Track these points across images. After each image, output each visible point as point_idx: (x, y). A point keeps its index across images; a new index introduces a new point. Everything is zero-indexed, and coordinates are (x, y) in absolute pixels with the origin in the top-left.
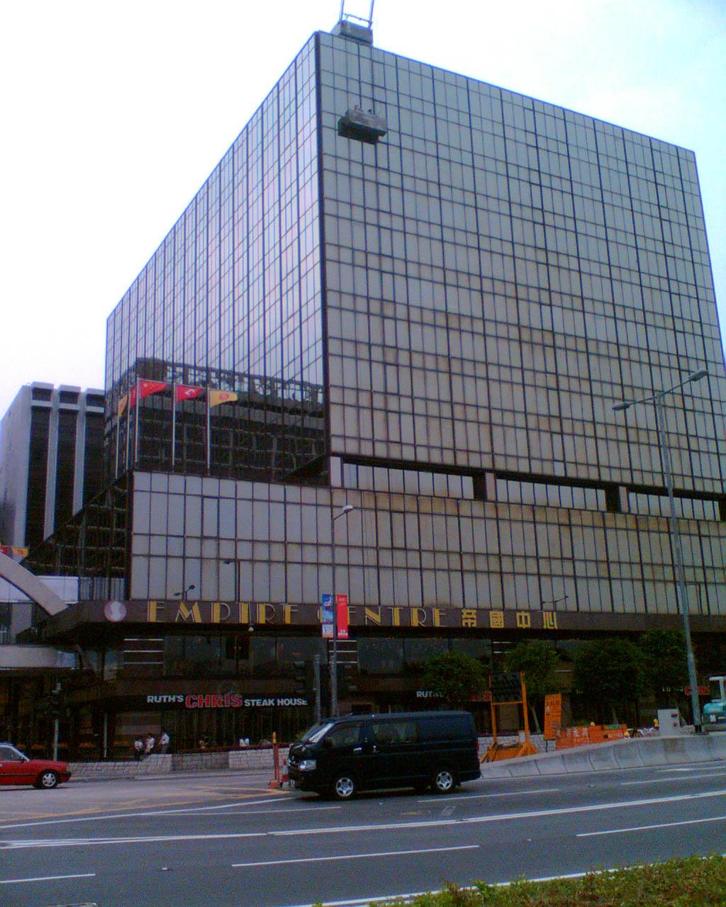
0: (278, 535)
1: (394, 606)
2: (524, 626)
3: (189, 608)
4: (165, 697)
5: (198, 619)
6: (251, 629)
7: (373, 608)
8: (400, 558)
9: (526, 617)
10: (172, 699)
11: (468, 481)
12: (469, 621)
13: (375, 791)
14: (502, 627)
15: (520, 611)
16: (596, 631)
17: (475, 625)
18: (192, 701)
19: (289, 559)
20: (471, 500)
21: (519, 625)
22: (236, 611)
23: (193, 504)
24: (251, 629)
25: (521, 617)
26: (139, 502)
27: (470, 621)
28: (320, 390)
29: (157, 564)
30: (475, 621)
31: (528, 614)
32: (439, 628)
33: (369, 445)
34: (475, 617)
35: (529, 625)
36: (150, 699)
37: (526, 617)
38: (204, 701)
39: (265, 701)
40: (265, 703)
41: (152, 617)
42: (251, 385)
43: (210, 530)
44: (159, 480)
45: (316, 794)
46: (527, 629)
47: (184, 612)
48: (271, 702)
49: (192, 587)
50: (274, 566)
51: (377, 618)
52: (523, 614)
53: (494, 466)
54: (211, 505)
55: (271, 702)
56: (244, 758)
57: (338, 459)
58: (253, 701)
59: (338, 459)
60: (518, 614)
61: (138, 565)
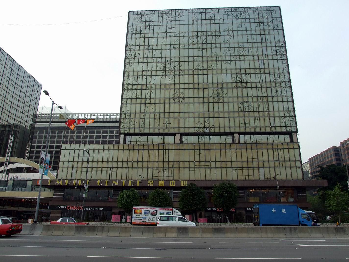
0: (100, 160)
1: (67, 179)
2: (172, 185)
3: (59, 181)
4: (61, 206)
5: (61, 184)
6: (278, 188)
7: (116, 180)
8: (140, 164)
9: (174, 182)
10: (213, 209)
11: (230, 137)
12: (150, 184)
13: (289, 240)
14: (163, 186)
15: (171, 180)
16: (257, 187)
17: (152, 185)
18: (69, 208)
19: (270, 166)
20: (179, 144)
21: (170, 185)
22: (72, 182)
23: (77, 152)
24: (76, 187)
25: (171, 182)
26: (62, 152)
27: (150, 184)
28: (119, 114)
29: (65, 169)
30: (153, 184)
31: (175, 182)
32: (50, 186)
33: (238, 128)
34: (153, 183)
35: (174, 185)
36: (57, 207)
37: (174, 182)
38: (72, 208)
39: (90, 208)
40: (90, 209)
41: (106, 185)
42: (97, 116)
43: (81, 159)
44: (68, 146)
45: (5, 236)
46: (173, 187)
47: (58, 182)
48: (92, 209)
49: (278, 175)
50: (144, 169)
51: (116, 184)
52: (172, 181)
53: (266, 131)
54: (81, 152)
55: (92, 209)
56: (214, 225)
57: (237, 134)
58: (86, 208)
59: (237, 134)
60: (170, 182)
61: (60, 169)
